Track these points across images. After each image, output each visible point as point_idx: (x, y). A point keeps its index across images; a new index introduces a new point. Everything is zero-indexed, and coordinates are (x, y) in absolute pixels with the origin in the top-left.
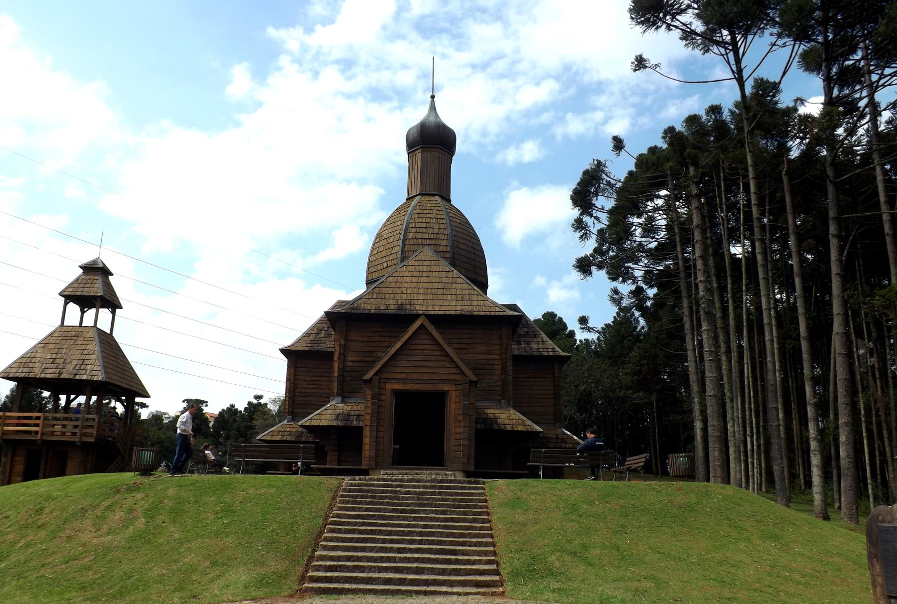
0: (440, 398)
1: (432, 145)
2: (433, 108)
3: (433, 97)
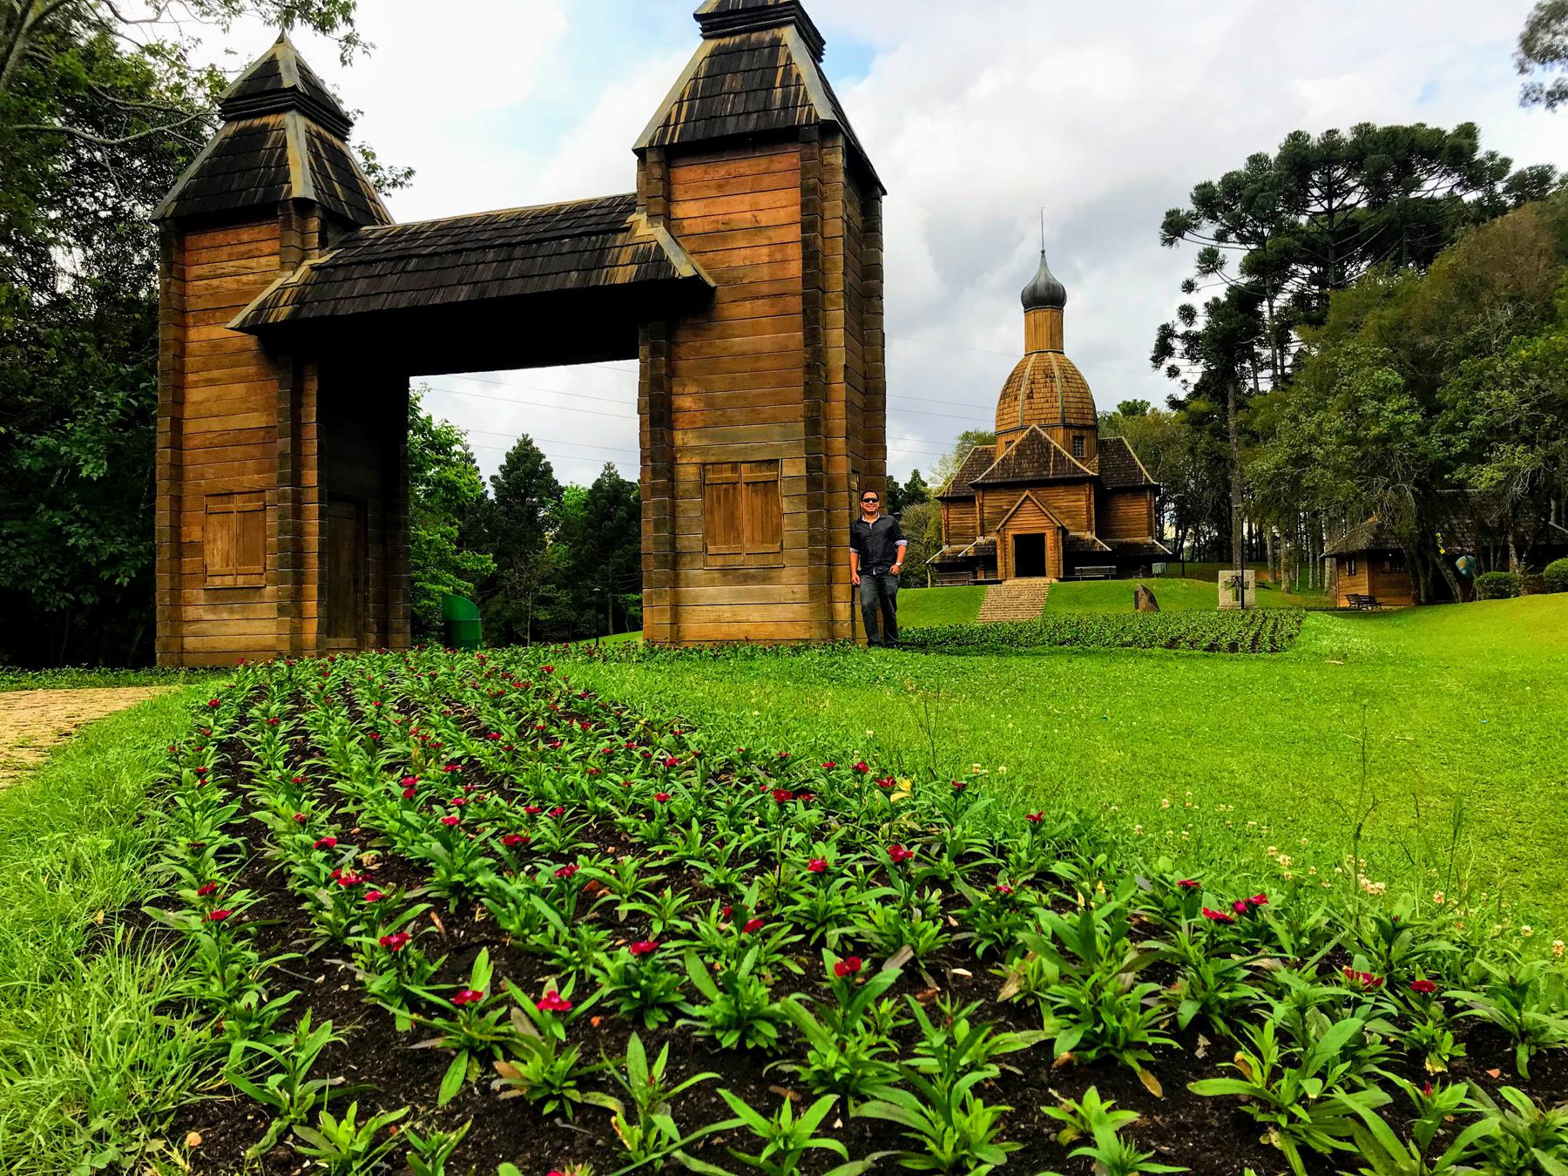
2: (1044, 264)
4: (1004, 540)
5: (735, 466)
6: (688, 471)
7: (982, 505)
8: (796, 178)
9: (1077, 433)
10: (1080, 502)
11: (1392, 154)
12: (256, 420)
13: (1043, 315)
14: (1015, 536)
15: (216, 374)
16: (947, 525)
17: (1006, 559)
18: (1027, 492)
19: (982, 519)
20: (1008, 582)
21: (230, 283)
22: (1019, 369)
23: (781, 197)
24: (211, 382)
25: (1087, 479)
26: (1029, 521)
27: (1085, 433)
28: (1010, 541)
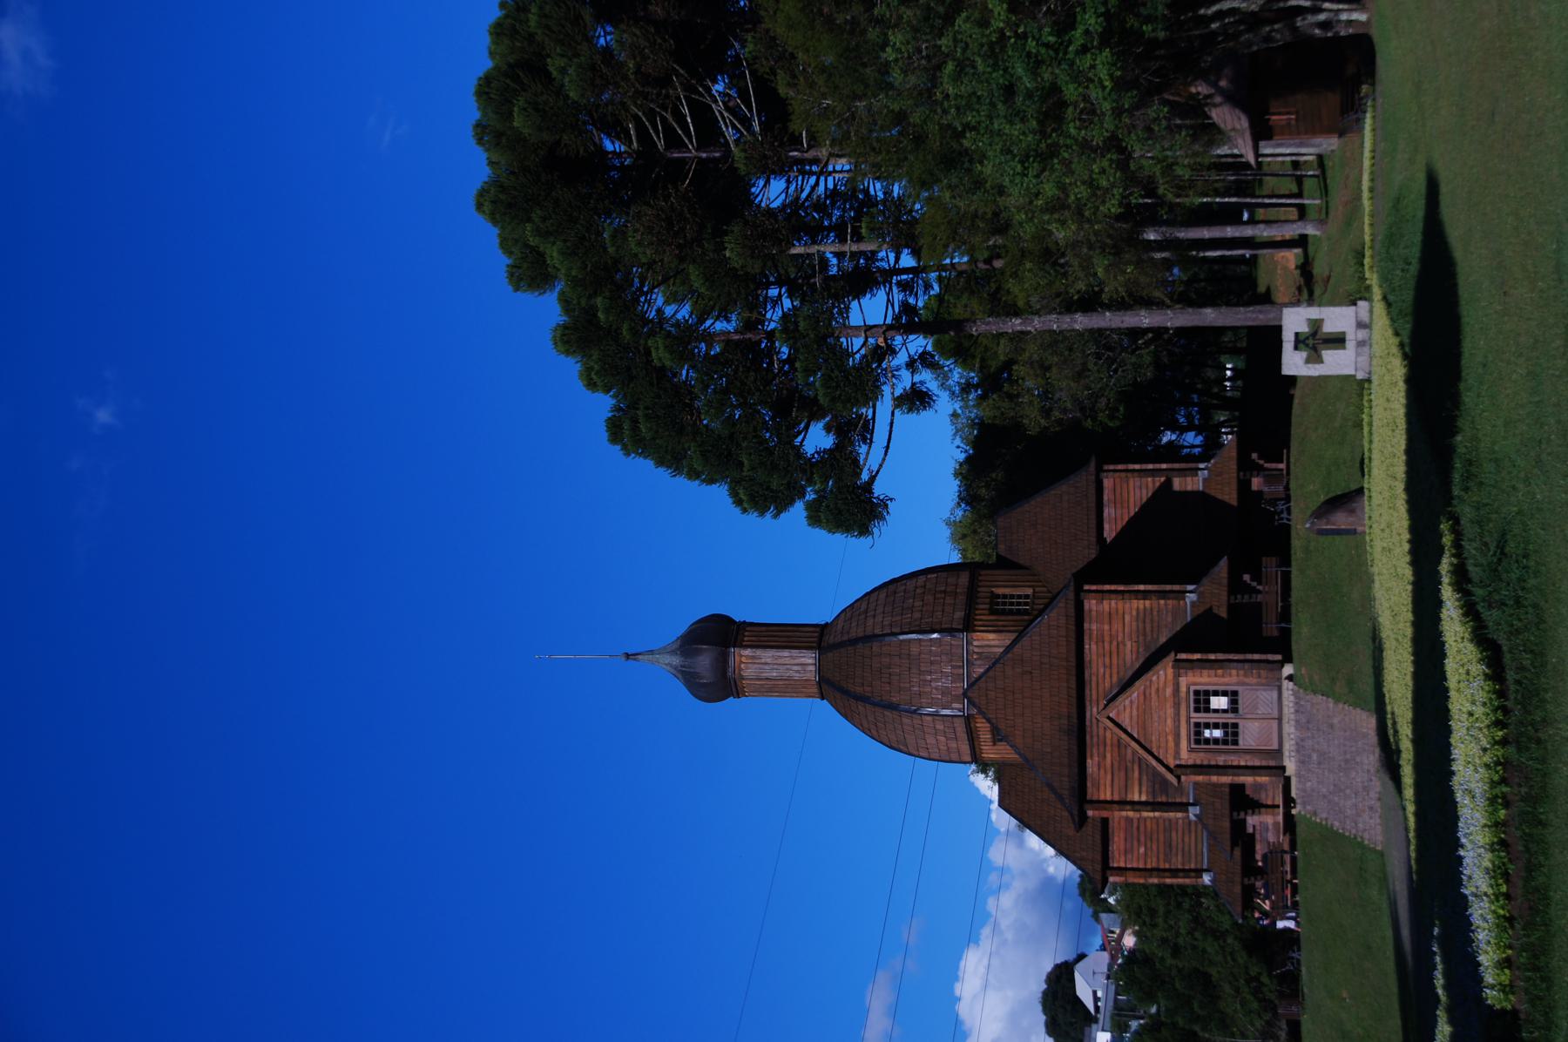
3: (628, 656)
9: (983, 606)
27: (983, 591)
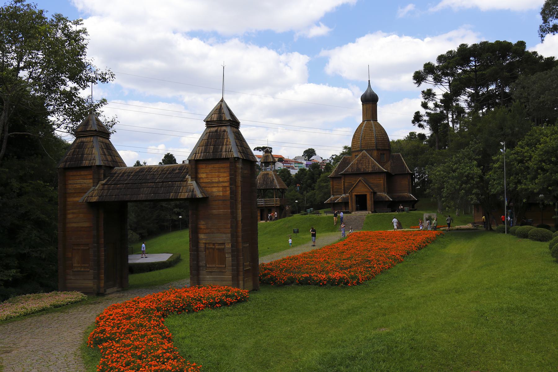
0: (365, 195)
1: (370, 101)
4: (351, 196)
5: (214, 244)
6: (202, 246)
7: (344, 182)
8: (229, 170)
10: (381, 181)
11: (503, 48)
12: (86, 224)
13: (369, 106)
14: (356, 196)
15: (75, 211)
16: (333, 188)
17: (352, 204)
18: (360, 178)
19: (344, 187)
20: (353, 213)
21: (78, 186)
22: (361, 126)
23: (225, 175)
24: (73, 213)
25: (383, 172)
26: (361, 190)
28: (354, 198)
